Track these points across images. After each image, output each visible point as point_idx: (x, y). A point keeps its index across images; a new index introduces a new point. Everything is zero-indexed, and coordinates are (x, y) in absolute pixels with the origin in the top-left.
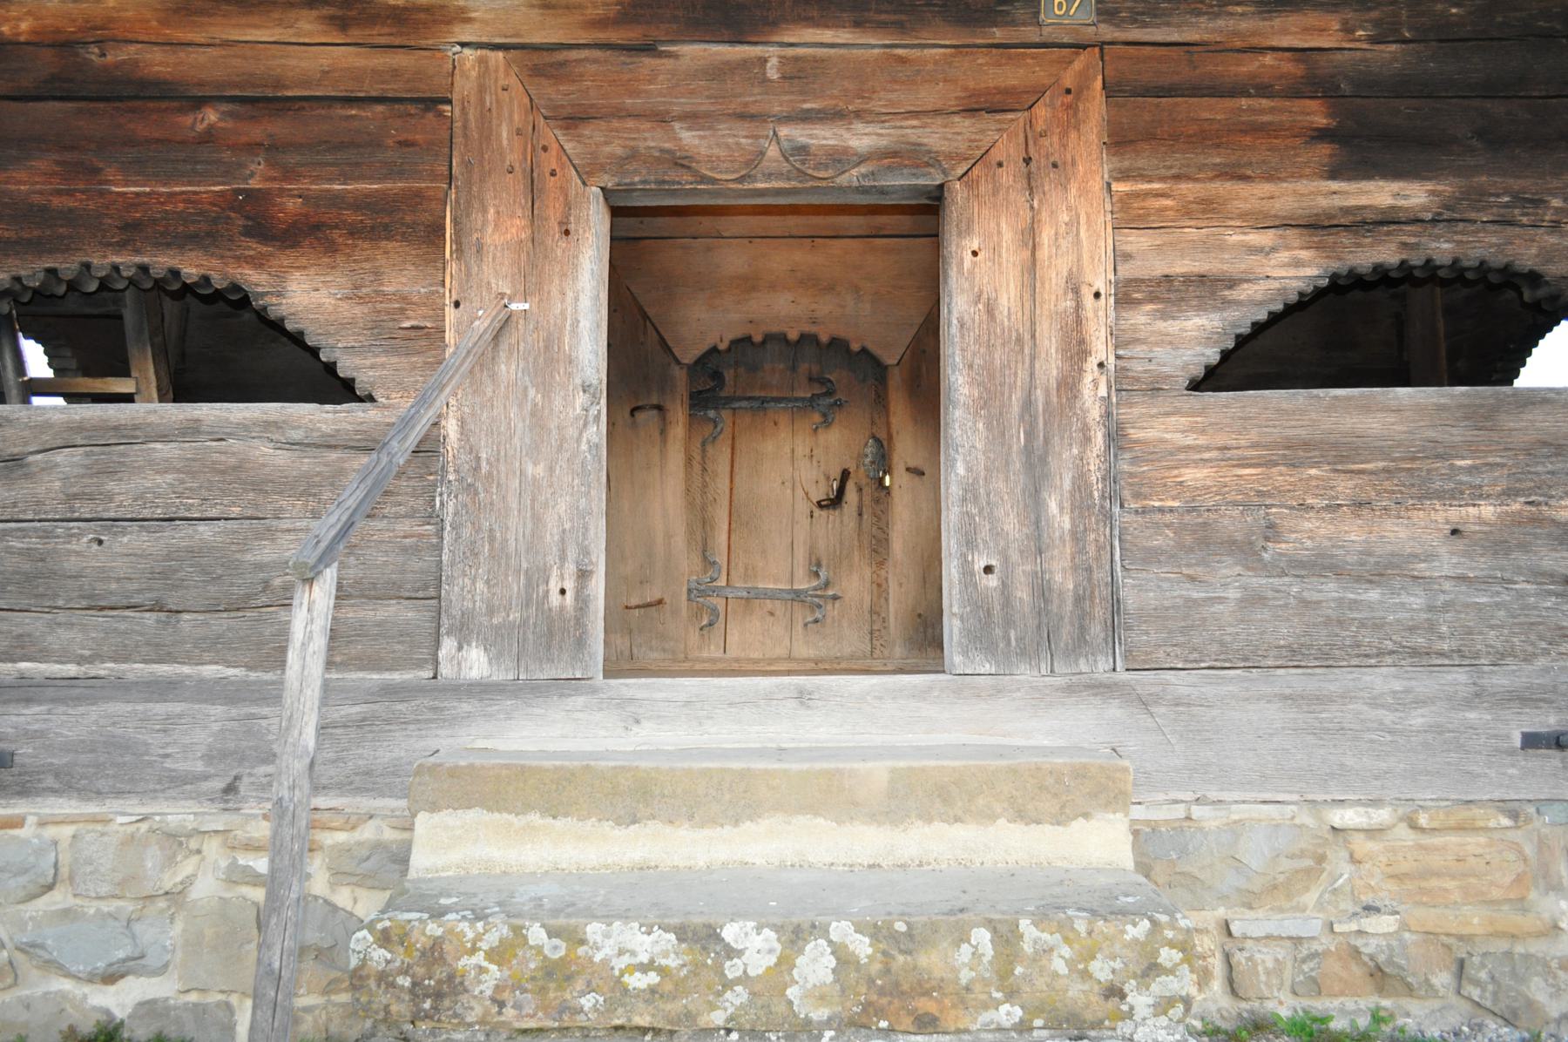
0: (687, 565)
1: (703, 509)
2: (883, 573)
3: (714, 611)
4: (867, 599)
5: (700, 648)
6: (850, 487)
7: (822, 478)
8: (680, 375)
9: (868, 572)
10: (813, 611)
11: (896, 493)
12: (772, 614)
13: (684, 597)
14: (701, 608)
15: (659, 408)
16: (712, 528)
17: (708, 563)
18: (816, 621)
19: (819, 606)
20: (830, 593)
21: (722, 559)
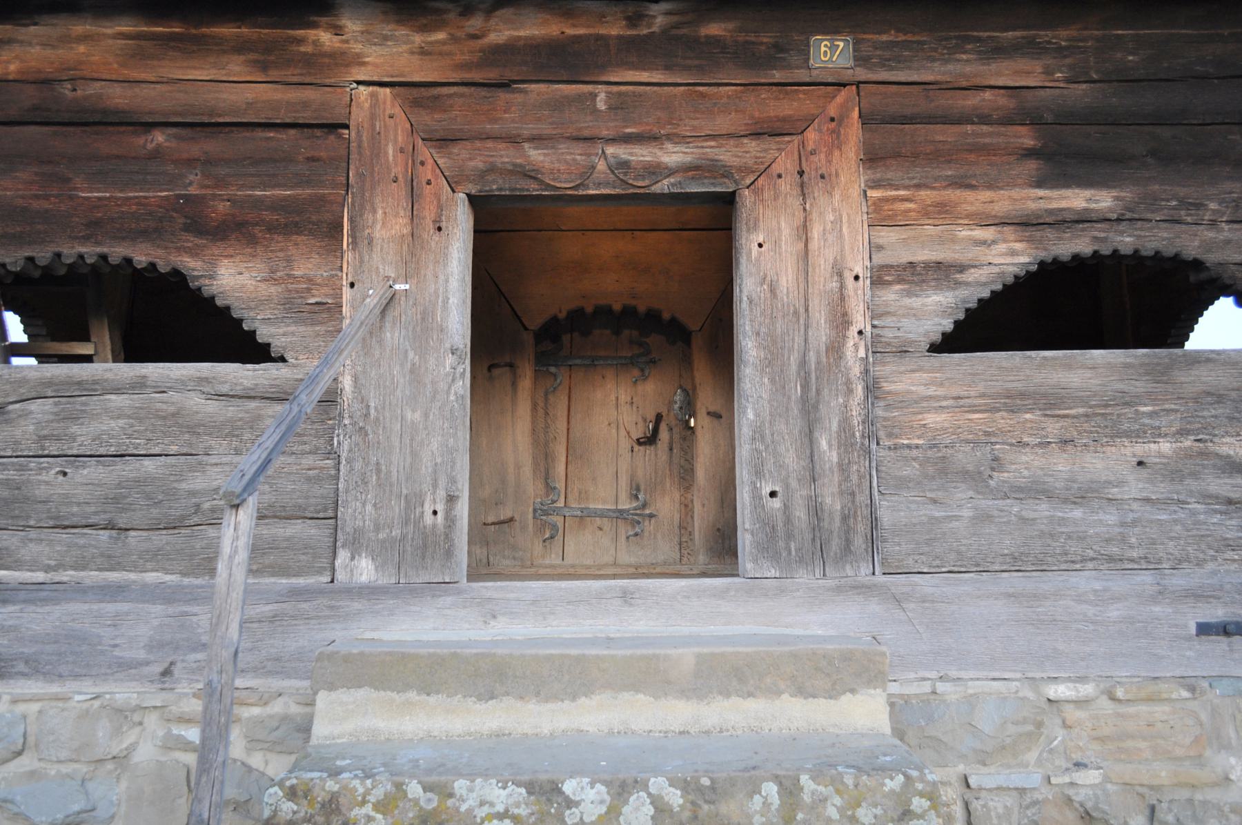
0: (532, 489)
1: (546, 444)
2: (689, 496)
3: (554, 527)
4: (677, 516)
5: (543, 557)
6: (663, 428)
7: (640, 420)
8: (528, 338)
9: (677, 495)
10: (634, 527)
11: (699, 432)
12: (601, 529)
13: (530, 516)
14: (544, 524)
15: (511, 365)
16: (553, 460)
17: (550, 488)
18: (636, 535)
19: (639, 523)
20: (647, 512)
21: (560, 485)
